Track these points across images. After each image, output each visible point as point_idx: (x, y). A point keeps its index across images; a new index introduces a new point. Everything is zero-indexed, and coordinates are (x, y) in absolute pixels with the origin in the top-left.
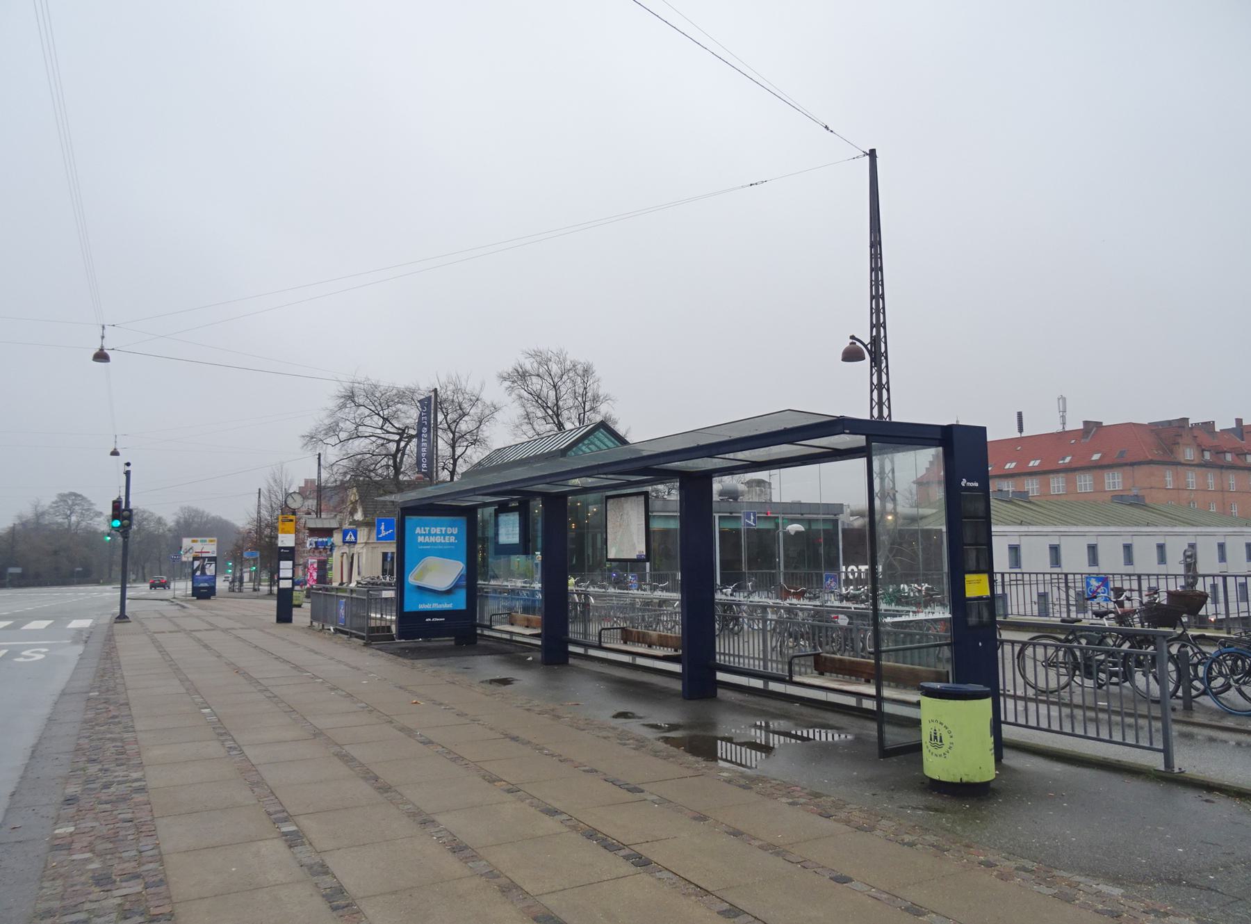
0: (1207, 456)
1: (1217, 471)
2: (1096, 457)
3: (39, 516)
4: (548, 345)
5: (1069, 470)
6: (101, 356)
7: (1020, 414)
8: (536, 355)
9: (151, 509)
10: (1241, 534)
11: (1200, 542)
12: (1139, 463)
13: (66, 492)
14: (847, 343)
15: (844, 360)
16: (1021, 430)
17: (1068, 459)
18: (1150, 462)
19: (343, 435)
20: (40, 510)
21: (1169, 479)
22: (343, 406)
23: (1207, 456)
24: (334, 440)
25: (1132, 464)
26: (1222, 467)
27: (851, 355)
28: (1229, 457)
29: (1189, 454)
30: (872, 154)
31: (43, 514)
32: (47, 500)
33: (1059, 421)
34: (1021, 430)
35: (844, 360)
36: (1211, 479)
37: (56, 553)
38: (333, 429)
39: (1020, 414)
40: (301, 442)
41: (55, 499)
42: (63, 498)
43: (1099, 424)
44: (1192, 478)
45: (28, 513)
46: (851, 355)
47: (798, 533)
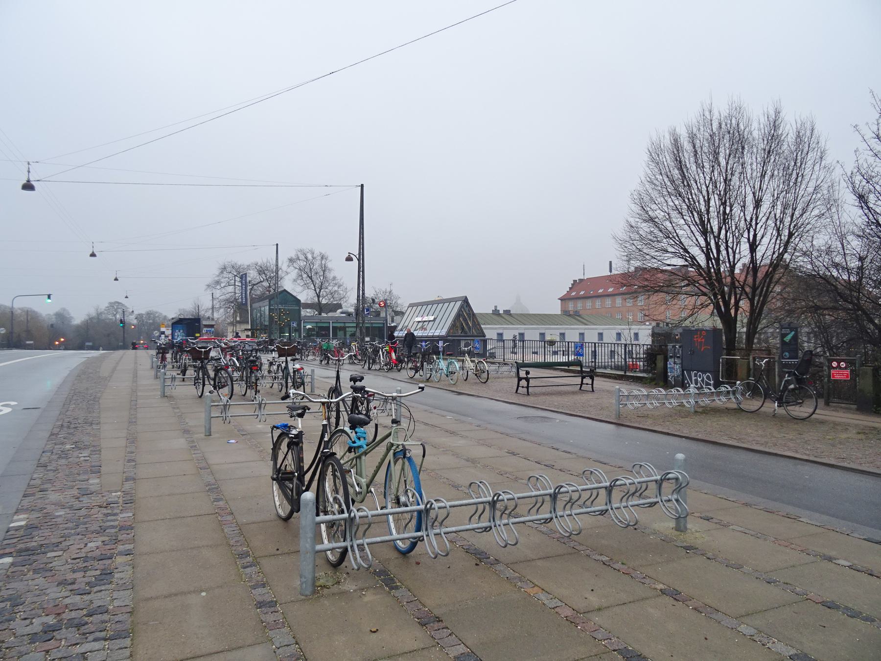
2: (601, 291)
3: (99, 314)
4: (306, 247)
6: (116, 279)
7: (611, 262)
8: (301, 251)
9: (160, 311)
10: (615, 329)
13: (113, 301)
16: (611, 271)
19: (223, 285)
20: (99, 311)
22: (222, 272)
24: (218, 287)
27: (349, 259)
31: (101, 313)
32: (103, 305)
34: (611, 271)
37: (108, 335)
38: (218, 283)
39: (611, 262)
40: (205, 287)
41: (107, 305)
42: (112, 305)
45: (93, 313)
46: (349, 259)
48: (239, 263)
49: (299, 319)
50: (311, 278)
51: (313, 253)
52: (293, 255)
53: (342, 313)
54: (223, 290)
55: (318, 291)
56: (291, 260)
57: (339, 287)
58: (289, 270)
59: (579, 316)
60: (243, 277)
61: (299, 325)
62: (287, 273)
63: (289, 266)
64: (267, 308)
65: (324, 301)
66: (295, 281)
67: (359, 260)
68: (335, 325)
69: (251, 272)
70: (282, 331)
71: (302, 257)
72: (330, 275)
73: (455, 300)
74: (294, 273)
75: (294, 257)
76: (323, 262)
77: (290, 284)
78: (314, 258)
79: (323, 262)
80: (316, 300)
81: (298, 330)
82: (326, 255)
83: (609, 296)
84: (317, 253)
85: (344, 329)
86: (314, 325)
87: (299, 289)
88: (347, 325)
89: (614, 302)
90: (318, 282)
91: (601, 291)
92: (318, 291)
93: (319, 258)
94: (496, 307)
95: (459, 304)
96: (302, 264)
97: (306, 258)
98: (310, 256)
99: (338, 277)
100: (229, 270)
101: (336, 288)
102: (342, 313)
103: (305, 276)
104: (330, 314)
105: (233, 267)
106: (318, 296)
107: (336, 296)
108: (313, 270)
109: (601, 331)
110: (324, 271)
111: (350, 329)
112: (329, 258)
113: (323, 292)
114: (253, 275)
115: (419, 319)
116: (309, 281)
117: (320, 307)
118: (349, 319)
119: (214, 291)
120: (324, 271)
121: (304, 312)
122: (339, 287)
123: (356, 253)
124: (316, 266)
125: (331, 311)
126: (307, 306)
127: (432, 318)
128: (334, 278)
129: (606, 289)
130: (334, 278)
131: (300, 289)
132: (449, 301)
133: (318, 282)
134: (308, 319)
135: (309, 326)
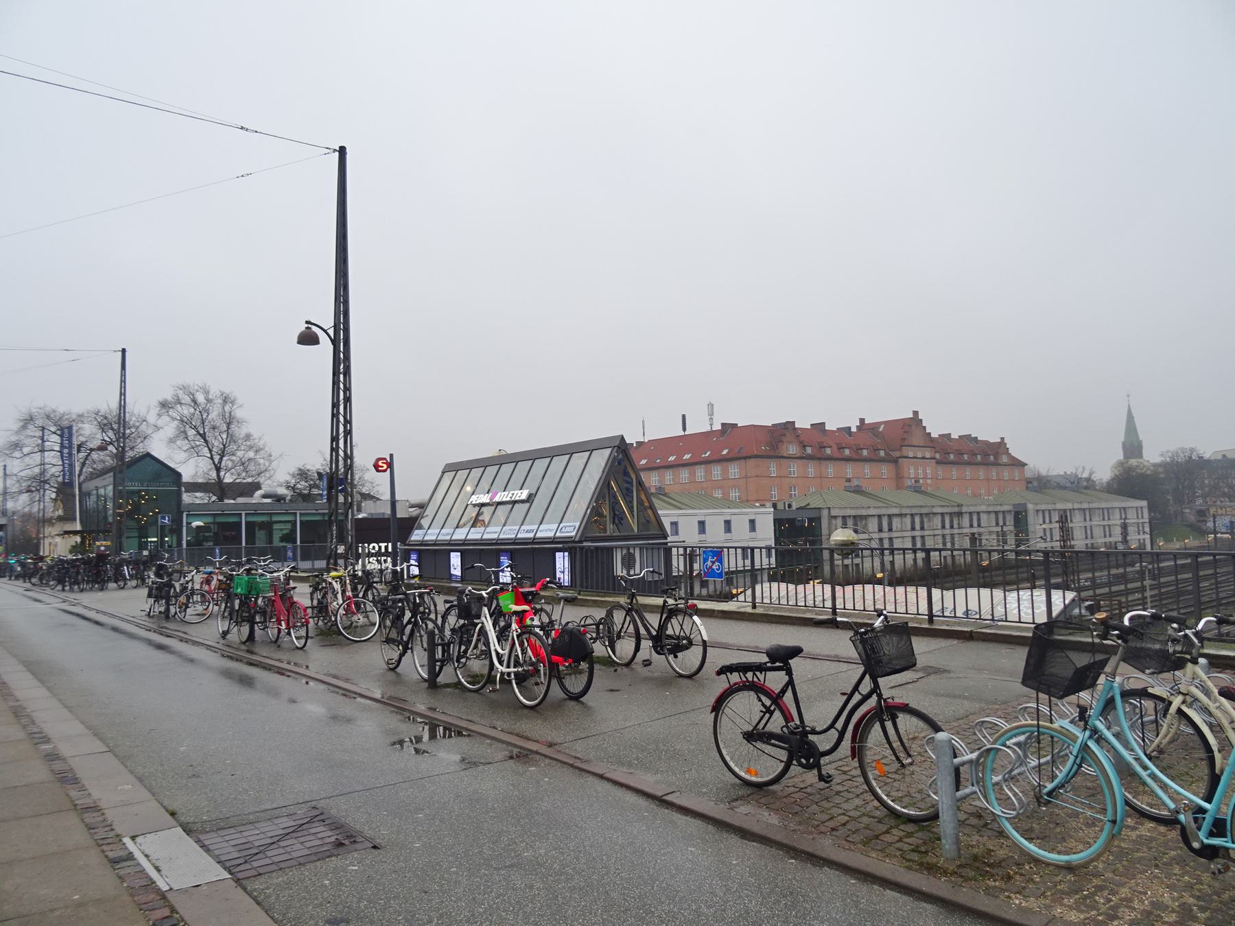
0: (952, 456)
1: (816, 462)
2: (672, 458)
4: (194, 381)
5: (707, 462)
7: (684, 416)
8: (183, 388)
10: (721, 514)
11: (734, 520)
12: (750, 457)
14: (302, 327)
15: (299, 343)
16: (684, 429)
17: (725, 452)
18: (756, 457)
19: (26, 450)
21: (1005, 474)
22: (24, 427)
23: (809, 450)
24: (17, 454)
25: (745, 458)
26: (820, 459)
27: (308, 338)
28: (966, 457)
29: (793, 450)
30: (342, 151)
33: (708, 423)
34: (684, 429)
35: (299, 343)
36: (811, 469)
38: (16, 446)
39: (684, 416)
43: (734, 426)
44: (794, 468)
46: (308, 338)
47: (198, 527)
48: (61, 410)
49: (178, 510)
50: (203, 436)
51: (207, 393)
52: (168, 396)
53: (264, 496)
54: (27, 459)
55: (217, 458)
56: (164, 405)
57: (257, 452)
58: (160, 423)
59: (665, 495)
60: (66, 432)
61: (177, 521)
62: (157, 428)
63: (160, 415)
64: (110, 488)
65: (228, 479)
66: (172, 441)
67: (335, 342)
68: (251, 519)
69: (86, 426)
70: (143, 533)
71: (187, 399)
72: (240, 432)
73: (590, 447)
74: (170, 429)
75: (169, 398)
76: (227, 408)
77: (162, 445)
78: (208, 401)
79: (227, 408)
80: (214, 474)
81: (176, 530)
82: (232, 397)
83: (685, 465)
84: (214, 391)
85: (268, 527)
86: (210, 520)
87: (182, 456)
88: (275, 518)
89: (693, 474)
90: (217, 445)
91: (672, 458)
92: (217, 458)
93: (220, 401)
94: (1002, 439)
95: (601, 459)
96: (186, 411)
97: (194, 401)
98: (201, 398)
99: (256, 435)
100: (39, 422)
101: (251, 454)
102: (264, 496)
103: (191, 432)
104: (241, 500)
105: (48, 417)
106: (218, 469)
107: (252, 467)
108: (208, 422)
109: (702, 519)
110: (229, 425)
111: (282, 526)
112: (239, 402)
113: (226, 462)
114: (89, 432)
115: (485, 499)
116: (200, 442)
117: (220, 489)
118: (278, 508)
119: (9, 462)
120: (229, 425)
121: (187, 498)
122: (257, 452)
123: (328, 322)
124: (214, 415)
125: (241, 495)
126: (194, 487)
127: (524, 495)
128: (248, 437)
129: (680, 456)
130: (248, 437)
131: (184, 455)
132: (570, 450)
133: (217, 445)
134: (195, 511)
135: (197, 523)
